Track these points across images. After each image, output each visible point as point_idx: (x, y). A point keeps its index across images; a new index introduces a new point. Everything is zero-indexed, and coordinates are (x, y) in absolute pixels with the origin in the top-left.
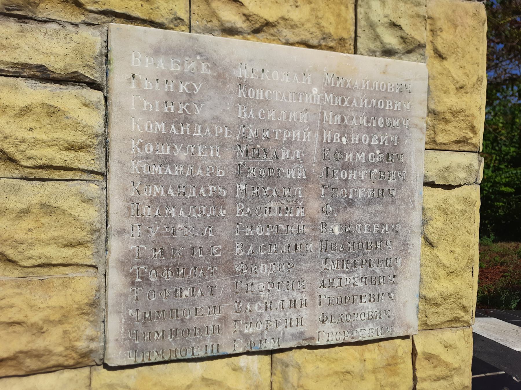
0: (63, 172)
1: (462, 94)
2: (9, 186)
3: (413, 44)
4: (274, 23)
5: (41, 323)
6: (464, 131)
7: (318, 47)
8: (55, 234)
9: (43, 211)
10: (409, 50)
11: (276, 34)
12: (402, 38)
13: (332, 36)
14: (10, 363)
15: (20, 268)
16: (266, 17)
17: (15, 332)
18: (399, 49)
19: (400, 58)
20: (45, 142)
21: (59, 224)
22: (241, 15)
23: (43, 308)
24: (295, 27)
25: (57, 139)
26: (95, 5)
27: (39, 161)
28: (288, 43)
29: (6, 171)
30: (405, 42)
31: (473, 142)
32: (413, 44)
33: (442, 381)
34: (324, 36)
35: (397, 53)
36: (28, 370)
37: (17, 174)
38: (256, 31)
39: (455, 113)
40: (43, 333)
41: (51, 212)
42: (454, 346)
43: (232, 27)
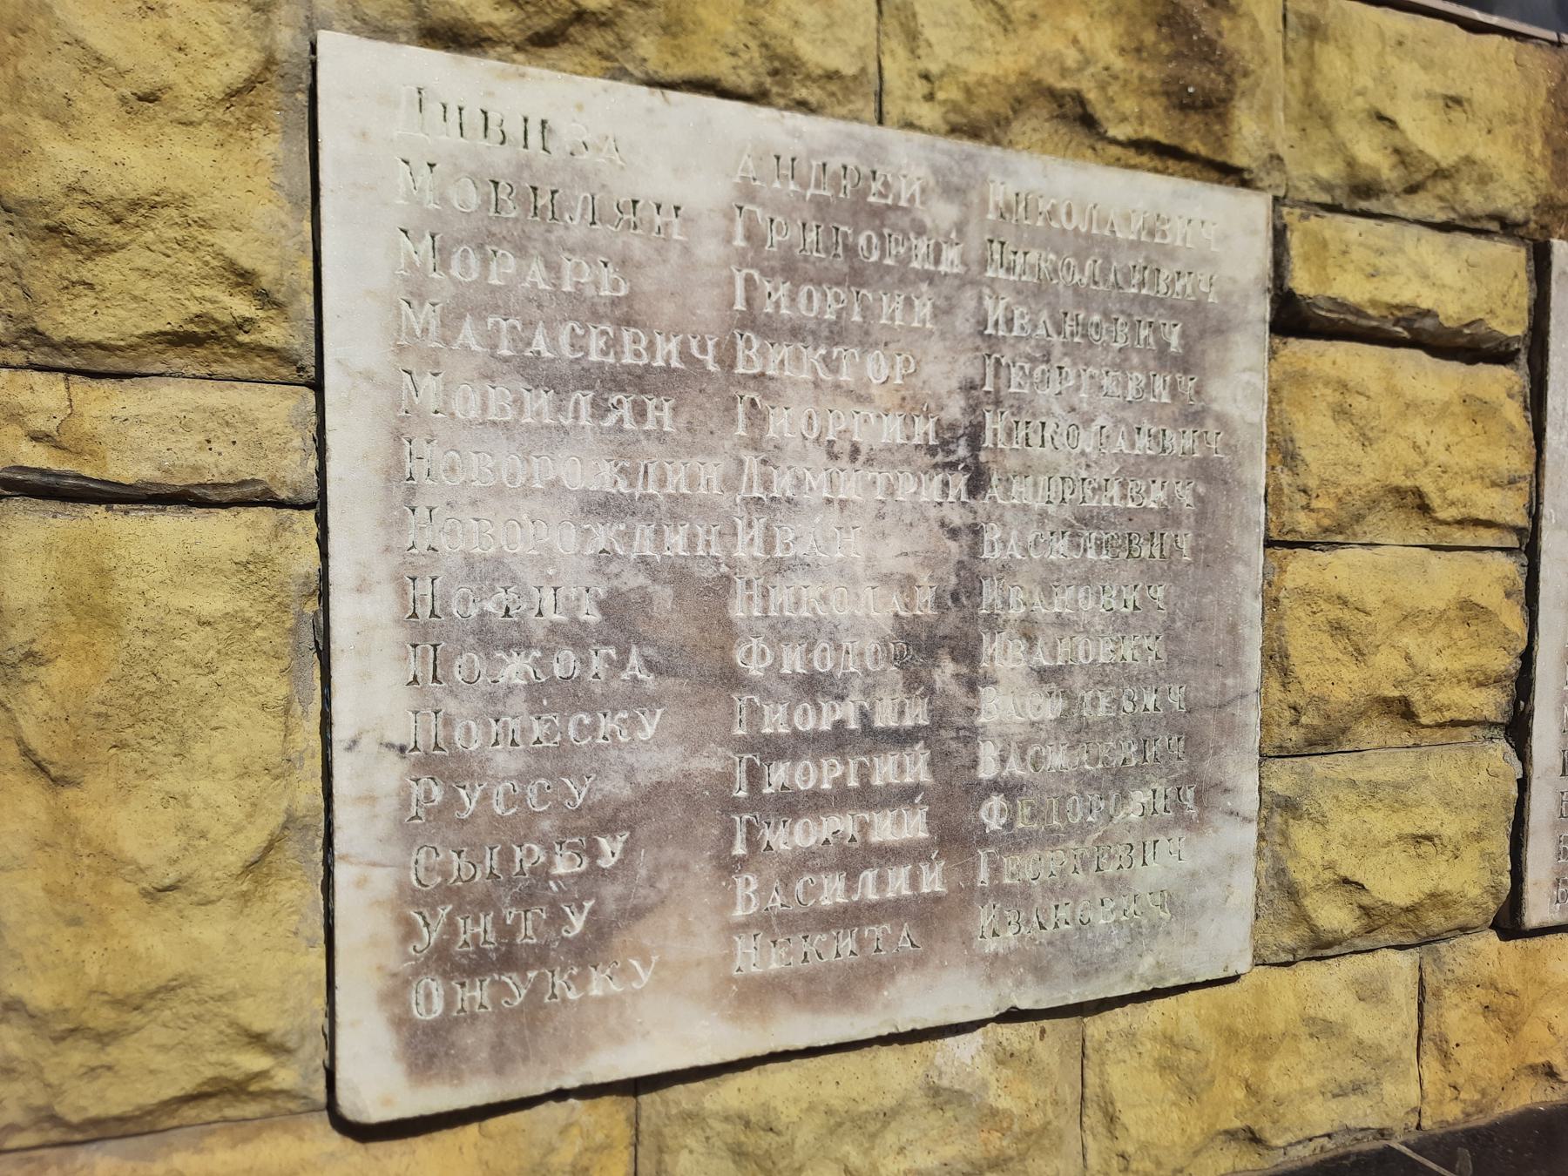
0: (1482, 531)
1: (160, 127)
4: (603, 14)
6: (198, 292)
7: (758, 97)
10: (537, 34)
11: (613, 51)
12: (1397, 151)
17: (1419, 856)
26: (1122, 125)
28: (653, 83)
30: (1403, 162)
31: (264, 342)
34: (777, 64)
35: (1385, 191)
39: (143, 206)
43: (457, 20)
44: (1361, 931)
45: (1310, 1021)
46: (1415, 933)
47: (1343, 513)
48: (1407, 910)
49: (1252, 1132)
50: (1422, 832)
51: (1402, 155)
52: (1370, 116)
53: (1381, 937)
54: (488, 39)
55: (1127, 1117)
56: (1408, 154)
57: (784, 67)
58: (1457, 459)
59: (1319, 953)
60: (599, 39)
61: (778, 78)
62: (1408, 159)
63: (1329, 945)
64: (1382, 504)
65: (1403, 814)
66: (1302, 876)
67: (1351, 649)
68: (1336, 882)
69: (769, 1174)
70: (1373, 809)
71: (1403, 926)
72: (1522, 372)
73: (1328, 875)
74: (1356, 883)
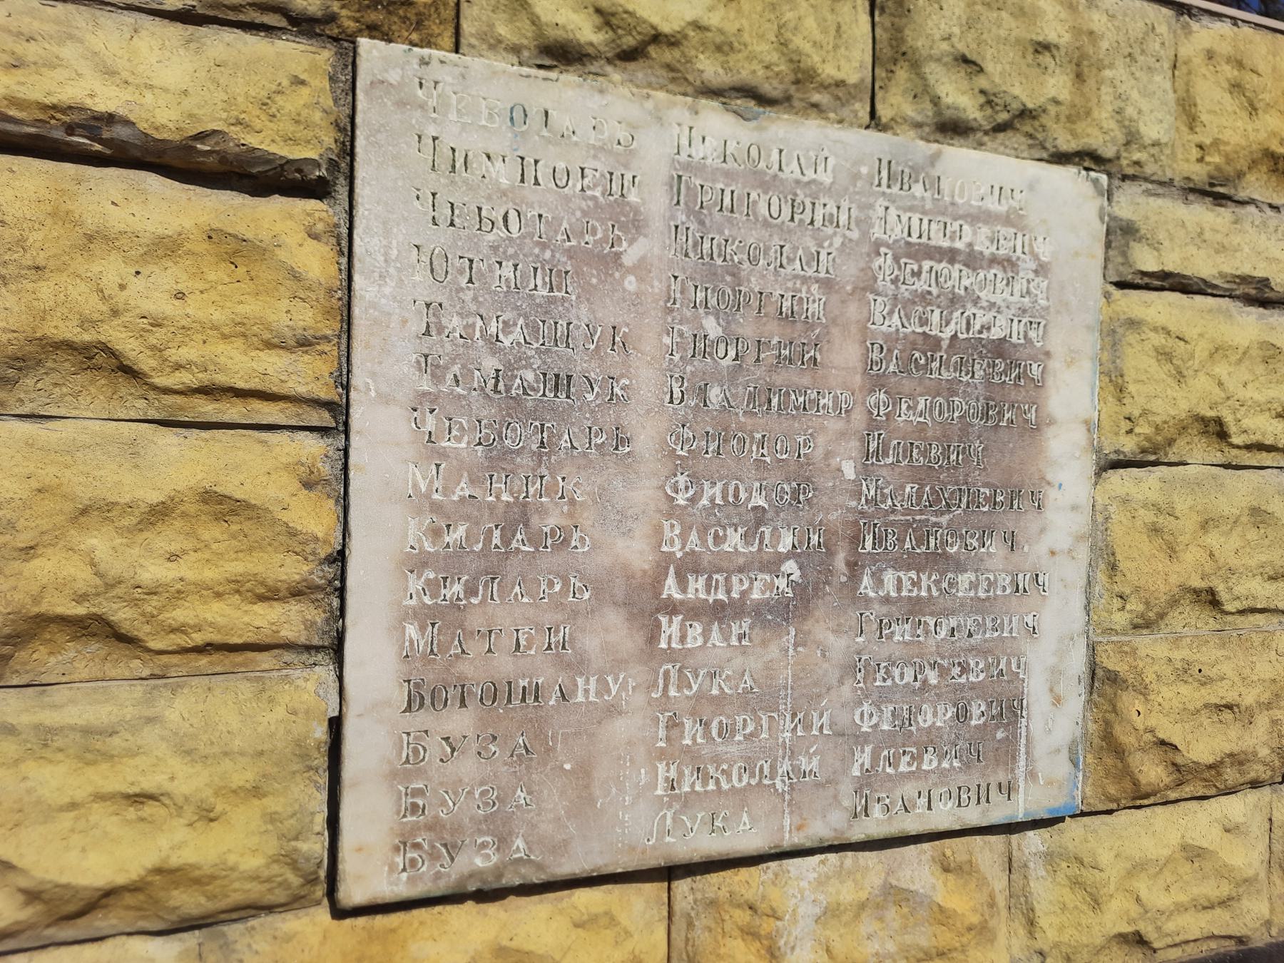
0: (256, 404)
2: (1214, 478)
3: (634, 33)
4: (673, 36)
5: (208, 793)
8: (1263, 558)
9: (1253, 519)
10: (624, 51)
11: (678, 65)
13: (819, 75)
14: (129, 899)
15: (147, 656)
16: (655, 20)
17: (142, 819)
18: (975, 119)
19: (980, 145)
20: (215, 327)
21: (1267, 542)
22: (591, 10)
23: (214, 756)
24: (726, 48)
25: (245, 321)
27: (200, 375)
29: (113, 403)
32: (634, 33)
33: (1218, 911)
36: (174, 918)
37: (139, 407)
38: (629, 56)
40: (212, 820)
41: (1261, 522)
42: (966, 868)
44: (1172, 785)
45: (1185, 848)
46: (1215, 786)
47: (1159, 438)
48: (1210, 767)
49: (1140, 936)
50: (1224, 702)
51: (989, 100)
52: (956, 59)
53: (1187, 789)
54: (588, 55)
55: (1043, 922)
56: (613, 15)
57: (804, 77)
58: (1251, 393)
59: (1138, 802)
60: (668, 55)
61: (800, 86)
62: (614, 21)
63: (1147, 796)
64: (1190, 431)
65: (1209, 686)
66: (1127, 739)
67: (1164, 547)
68: (1155, 743)
69: (773, 953)
70: (1186, 682)
71: (1205, 780)
72: (338, 208)
73: (1148, 737)
74: (1171, 745)
